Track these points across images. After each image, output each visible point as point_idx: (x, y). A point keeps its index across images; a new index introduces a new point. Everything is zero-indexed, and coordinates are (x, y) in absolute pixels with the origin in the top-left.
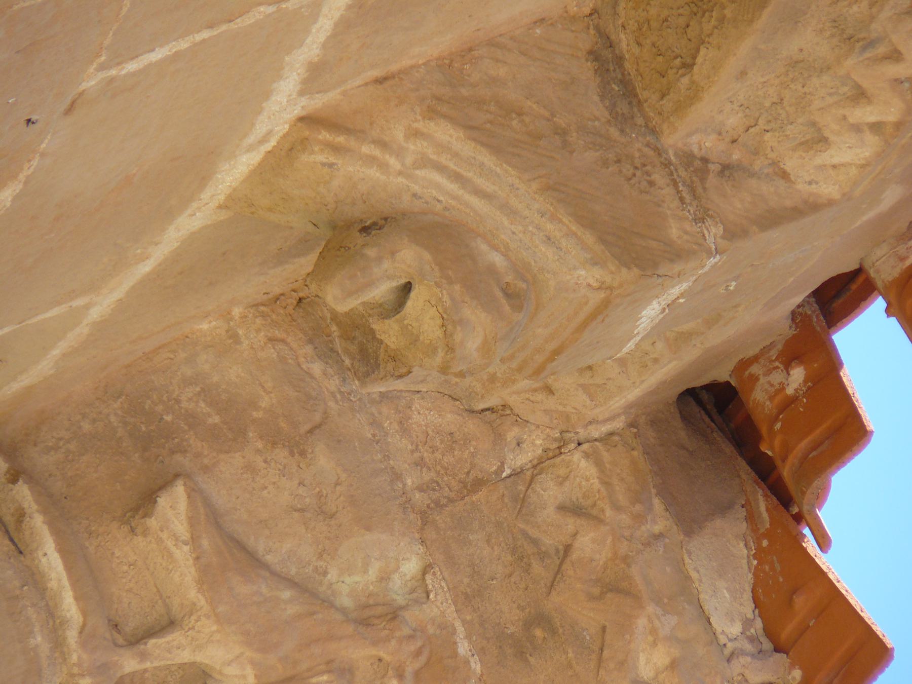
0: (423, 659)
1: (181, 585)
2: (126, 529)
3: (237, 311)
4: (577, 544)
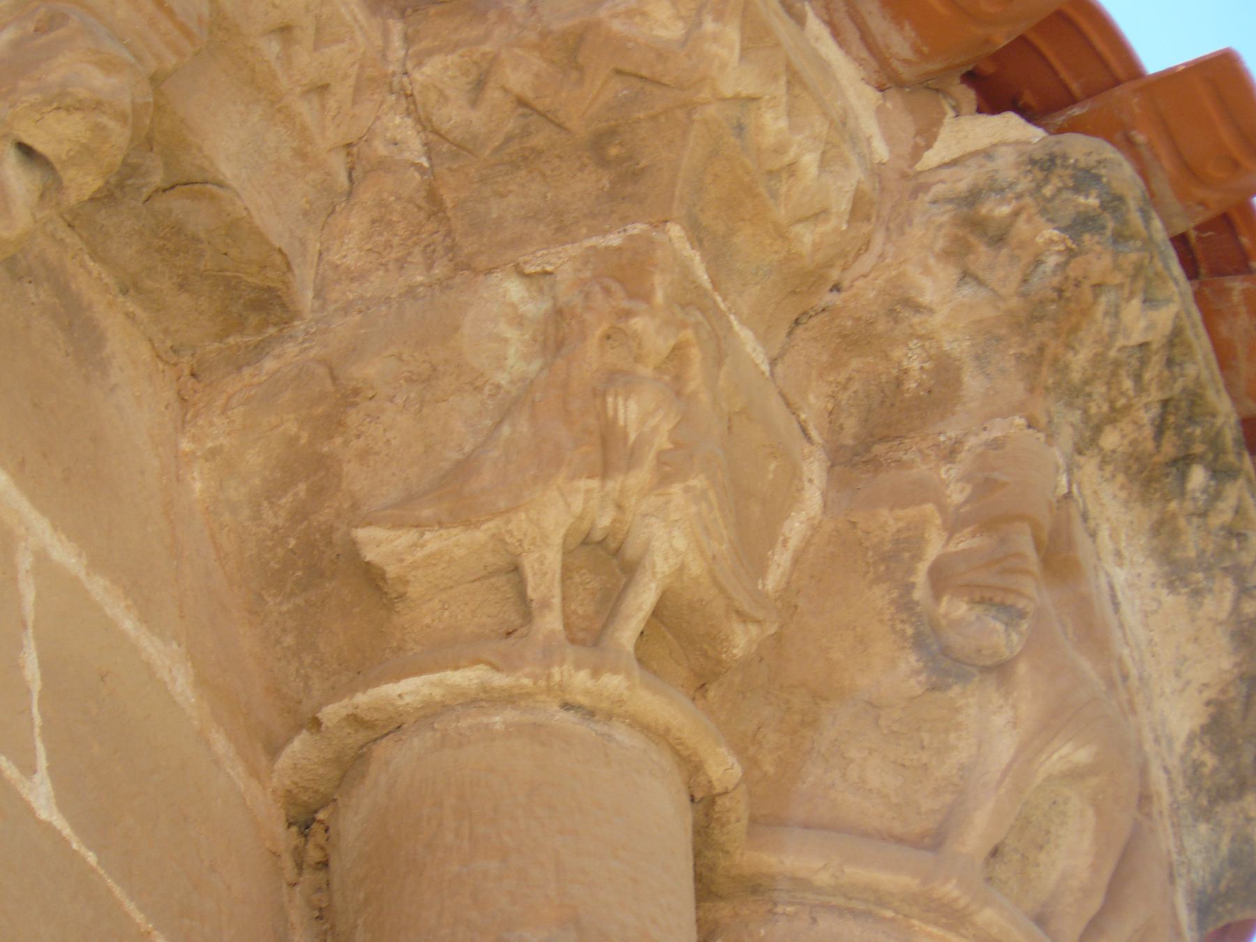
0: (615, 286)
2: (399, 606)
3: (186, 445)
4: (517, 89)
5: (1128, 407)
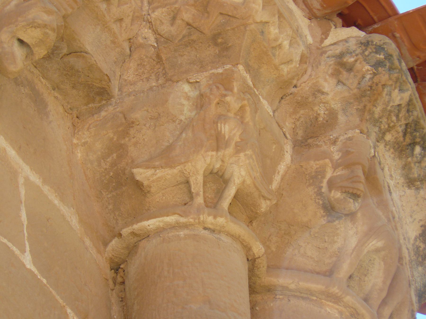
0: (220, 86)
1: (172, 175)
2: (148, 195)
4: (187, 20)
5: (394, 126)
